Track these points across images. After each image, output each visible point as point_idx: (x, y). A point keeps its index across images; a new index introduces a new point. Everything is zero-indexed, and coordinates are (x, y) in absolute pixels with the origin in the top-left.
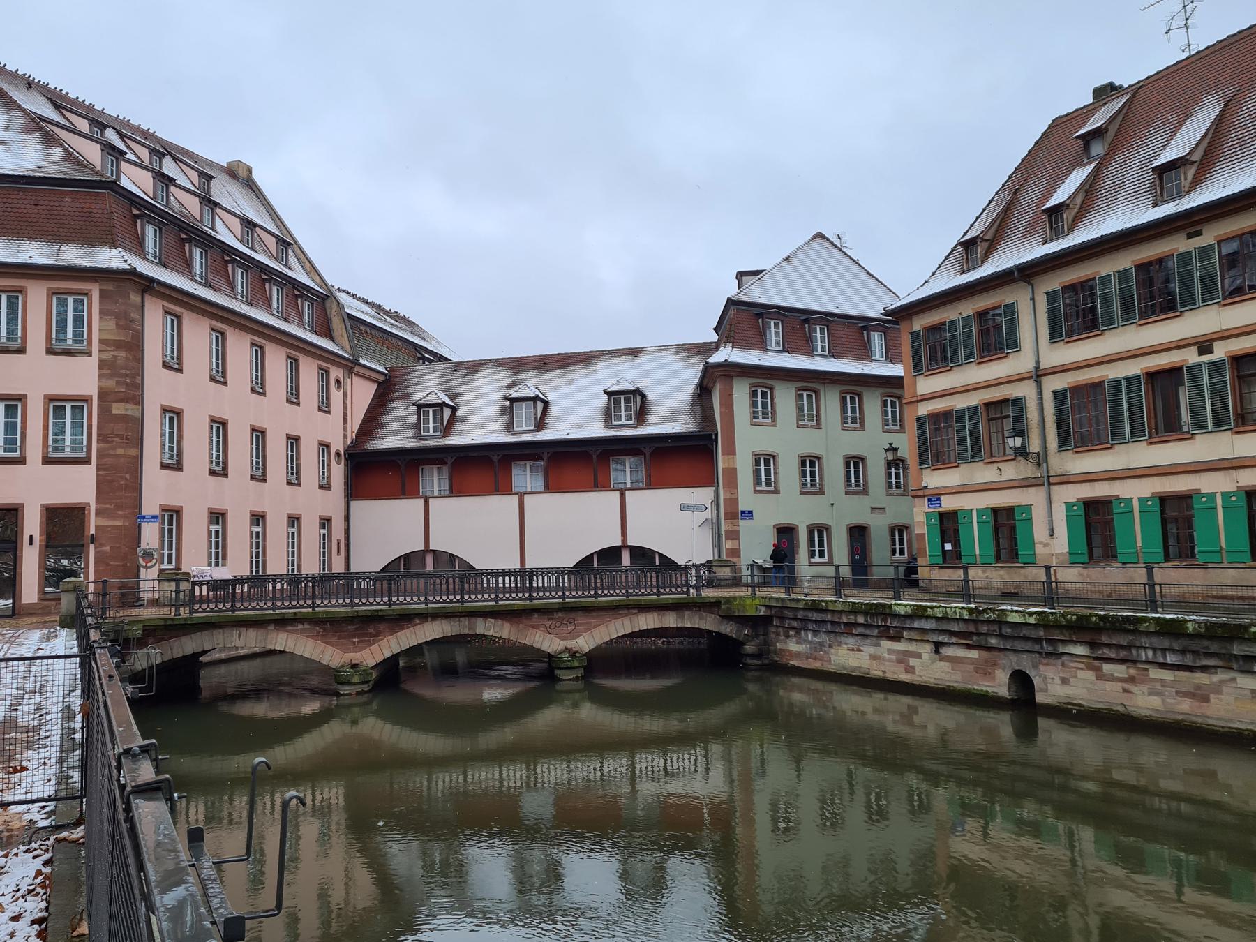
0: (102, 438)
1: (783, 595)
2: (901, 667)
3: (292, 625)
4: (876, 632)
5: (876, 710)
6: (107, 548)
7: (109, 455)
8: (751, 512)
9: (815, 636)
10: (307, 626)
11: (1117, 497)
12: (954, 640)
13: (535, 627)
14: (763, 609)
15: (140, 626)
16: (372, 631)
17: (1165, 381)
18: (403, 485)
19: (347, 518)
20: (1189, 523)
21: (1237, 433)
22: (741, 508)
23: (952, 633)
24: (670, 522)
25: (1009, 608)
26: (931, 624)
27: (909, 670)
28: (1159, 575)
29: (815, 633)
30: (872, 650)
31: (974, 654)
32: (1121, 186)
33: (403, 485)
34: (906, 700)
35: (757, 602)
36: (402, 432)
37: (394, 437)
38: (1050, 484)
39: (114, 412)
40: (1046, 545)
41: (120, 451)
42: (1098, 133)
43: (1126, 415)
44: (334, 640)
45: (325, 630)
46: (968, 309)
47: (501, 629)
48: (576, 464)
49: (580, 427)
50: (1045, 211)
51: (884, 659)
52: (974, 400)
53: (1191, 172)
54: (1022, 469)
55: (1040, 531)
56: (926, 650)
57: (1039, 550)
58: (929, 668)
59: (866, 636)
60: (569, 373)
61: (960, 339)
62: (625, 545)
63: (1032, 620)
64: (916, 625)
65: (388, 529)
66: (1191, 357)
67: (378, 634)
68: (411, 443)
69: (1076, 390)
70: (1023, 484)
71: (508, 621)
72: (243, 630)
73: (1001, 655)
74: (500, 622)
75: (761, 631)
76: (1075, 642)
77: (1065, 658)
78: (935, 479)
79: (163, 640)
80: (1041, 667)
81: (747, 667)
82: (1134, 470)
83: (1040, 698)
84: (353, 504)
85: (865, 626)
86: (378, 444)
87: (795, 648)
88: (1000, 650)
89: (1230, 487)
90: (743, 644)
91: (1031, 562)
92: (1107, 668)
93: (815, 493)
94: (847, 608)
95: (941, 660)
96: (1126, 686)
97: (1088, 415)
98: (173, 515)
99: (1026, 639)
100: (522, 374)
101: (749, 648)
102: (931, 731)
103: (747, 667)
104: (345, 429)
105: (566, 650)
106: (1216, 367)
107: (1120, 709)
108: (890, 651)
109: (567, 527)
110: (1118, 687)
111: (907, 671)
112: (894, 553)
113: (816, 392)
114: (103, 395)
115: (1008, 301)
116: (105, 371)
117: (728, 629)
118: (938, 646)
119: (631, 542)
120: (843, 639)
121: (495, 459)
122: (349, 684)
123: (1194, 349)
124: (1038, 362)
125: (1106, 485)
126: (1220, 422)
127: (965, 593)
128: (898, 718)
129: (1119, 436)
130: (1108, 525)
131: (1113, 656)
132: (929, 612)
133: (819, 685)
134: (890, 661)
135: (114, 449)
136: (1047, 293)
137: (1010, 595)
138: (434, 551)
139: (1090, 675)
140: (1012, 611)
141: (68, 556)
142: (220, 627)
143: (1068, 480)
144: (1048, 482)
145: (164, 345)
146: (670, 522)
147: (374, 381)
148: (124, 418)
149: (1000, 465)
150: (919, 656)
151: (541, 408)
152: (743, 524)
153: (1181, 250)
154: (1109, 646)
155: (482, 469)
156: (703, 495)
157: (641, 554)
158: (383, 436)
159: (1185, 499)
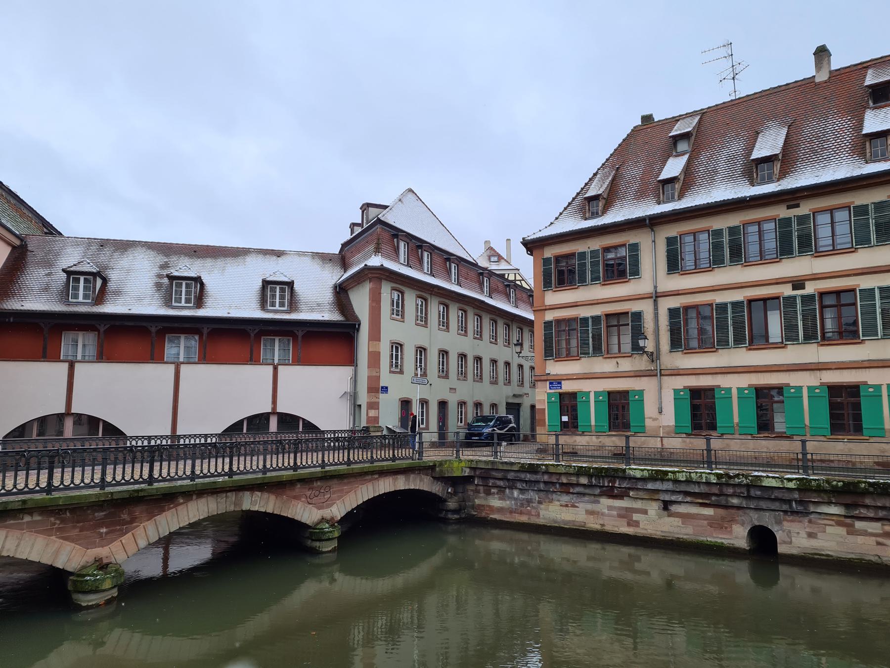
1: (492, 459)
2: (624, 522)
4: (597, 491)
5: (589, 558)
8: (387, 388)
9: (523, 494)
10: (37, 518)
11: (719, 386)
12: (689, 499)
13: (296, 498)
14: (468, 470)
17: (840, 298)
18: (45, 349)
20: (712, 408)
21: (822, 345)
22: (382, 384)
23: (687, 494)
24: (317, 393)
25: (764, 474)
26: (668, 486)
27: (637, 524)
28: (810, 446)
29: (522, 491)
30: (589, 507)
31: (709, 512)
32: (715, 172)
33: (45, 349)
34: (626, 551)
35: (463, 464)
36: (45, 296)
38: (661, 375)
40: (655, 419)
42: (685, 136)
43: (731, 329)
44: (75, 533)
45: (63, 521)
46: (595, 244)
47: (267, 503)
48: (230, 339)
50: (585, 198)
51: (603, 514)
52: (597, 311)
53: (678, 186)
54: (641, 363)
55: (650, 409)
56: (654, 508)
57: (648, 423)
58: (653, 521)
59: (584, 494)
60: (220, 262)
61: (588, 266)
62: (274, 412)
63: (791, 485)
64: (650, 486)
66: (787, 291)
67: (133, 520)
68: (57, 307)
69: (558, 322)
70: (638, 375)
71: (273, 493)
73: (740, 512)
74: (266, 495)
75: (460, 489)
76: (829, 503)
77: (812, 516)
78: (555, 368)
80: (785, 523)
81: (445, 521)
82: (730, 371)
83: (782, 549)
85: (590, 486)
86: (756, 154)
87: (496, 504)
88: (739, 508)
89: (816, 383)
90: (445, 501)
91: (642, 430)
92: (859, 525)
93: (443, 377)
94: (572, 470)
95: (669, 516)
96: (880, 540)
97: (692, 327)
99: (776, 499)
100: (174, 258)
101: (452, 504)
102: (656, 578)
103: (445, 521)
105: (323, 520)
106: (808, 299)
107: (874, 559)
108: (610, 508)
109: (221, 395)
110: (872, 541)
111: (629, 525)
113: (426, 300)
115: (632, 241)
117: (436, 488)
118: (666, 505)
119: (280, 409)
120: (554, 496)
121: (153, 330)
122: (96, 591)
123: (790, 286)
124: (656, 287)
125: (709, 377)
126: (810, 337)
127: (709, 460)
128: (616, 564)
129: (723, 343)
130: (625, 407)
131: (872, 515)
132: (670, 476)
133: (524, 536)
134: (609, 516)
136: (668, 239)
137: (769, 464)
139: (842, 531)
140: (768, 477)
143: (677, 373)
144: (657, 373)
146: (317, 393)
147: (9, 243)
149: (619, 360)
150: (645, 512)
151: (198, 289)
152: (382, 396)
153: (782, 216)
154: (867, 507)
156: (343, 373)
157: (288, 421)
158: (22, 298)
159: (854, 390)
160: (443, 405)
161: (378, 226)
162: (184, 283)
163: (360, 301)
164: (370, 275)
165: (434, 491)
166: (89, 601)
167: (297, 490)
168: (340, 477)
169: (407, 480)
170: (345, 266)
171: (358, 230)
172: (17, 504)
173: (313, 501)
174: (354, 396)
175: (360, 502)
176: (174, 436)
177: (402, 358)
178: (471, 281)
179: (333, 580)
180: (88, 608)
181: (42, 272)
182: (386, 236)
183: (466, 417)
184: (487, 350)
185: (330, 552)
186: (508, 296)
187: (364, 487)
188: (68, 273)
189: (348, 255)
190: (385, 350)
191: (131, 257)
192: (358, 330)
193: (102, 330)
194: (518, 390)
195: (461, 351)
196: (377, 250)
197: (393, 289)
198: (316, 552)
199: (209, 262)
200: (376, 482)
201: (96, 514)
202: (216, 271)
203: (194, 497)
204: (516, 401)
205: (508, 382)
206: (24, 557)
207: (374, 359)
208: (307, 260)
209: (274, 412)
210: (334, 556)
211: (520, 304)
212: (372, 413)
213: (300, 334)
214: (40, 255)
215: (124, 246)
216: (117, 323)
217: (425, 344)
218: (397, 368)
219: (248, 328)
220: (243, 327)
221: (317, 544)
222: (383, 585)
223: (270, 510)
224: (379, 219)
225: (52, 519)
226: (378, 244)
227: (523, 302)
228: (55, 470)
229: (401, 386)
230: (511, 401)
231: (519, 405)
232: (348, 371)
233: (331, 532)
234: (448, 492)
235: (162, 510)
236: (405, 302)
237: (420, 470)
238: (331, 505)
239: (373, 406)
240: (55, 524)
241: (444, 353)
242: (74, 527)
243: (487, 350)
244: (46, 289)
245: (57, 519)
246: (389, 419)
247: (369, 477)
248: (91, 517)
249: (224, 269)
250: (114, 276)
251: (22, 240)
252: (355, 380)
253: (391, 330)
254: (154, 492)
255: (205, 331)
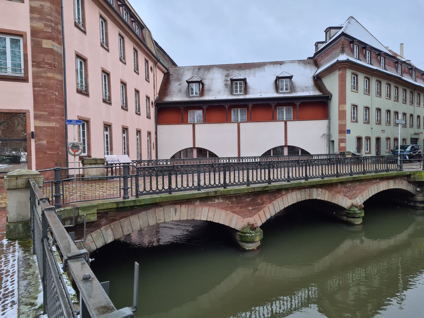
0: (36, 64)
3: (211, 200)
6: (44, 142)
7: (41, 77)
8: (350, 130)
10: (221, 201)
13: (339, 193)
15: (95, 211)
16: (259, 201)
19: (156, 133)
22: (347, 129)
37: (176, 96)
39: (44, 46)
41: (50, 75)
44: (237, 209)
45: (232, 203)
49: (264, 93)
60: (252, 71)
65: (176, 138)
67: (263, 203)
68: (186, 99)
71: (327, 189)
72: (178, 207)
74: (324, 191)
79: (114, 220)
84: (158, 126)
86: (168, 99)
98: (84, 123)
100: (231, 71)
103: (415, 208)
104: (154, 92)
105: (353, 206)
109: (261, 137)
112: (105, 154)
114: (34, 32)
116: (35, 15)
117: (410, 188)
119: (289, 144)
121: (227, 107)
135: (46, 73)
138: (197, 148)
141: (15, 150)
142: (161, 206)
145: (75, 14)
146: (308, 135)
148: (51, 51)
152: (347, 135)
155: (216, 111)
156: (322, 124)
157: (293, 150)
160: (378, 140)
161: (343, 37)
162: (238, 82)
163: (332, 84)
164: (339, 67)
165: (408, 190)
166: (249, 247)
167: (339, 188)
168: (360, 181)
169: (395, 183)
170: (317, 64)
171: (321, 46)
172: (213, 193)
173: (347, 195)
174: (329, 136)
175: (371, 196)
176: (239, 158)
177: (357, 114)
178: (392, 67)
179: (362, 241)
180: (249, 251)
181: (177, 84)
182: (347, 43)
183: (390, 147)
184: (402, 107)
185: (360, 224)
186: (411, 75)
187: (372, 187)
188: (189, 82)
189: (319, 59)
190: (348, 108)
191: (212, 73)
192: (330, 99)
193: (205, 108)
194: (417, 131)
195: (387, 109)
196: (343, 51)
197: (353, 74)
198: (351, 224)
199: (247, 71)
200: (378, 184)
201: (247, 199)
202: (251, 75)
203: (290, 191)
204: (416, 137)
205: (412, 126)
206: (217, 221)
207: (342, 115)
208: (296, 65)
209: (286, 146)
210: (361, 227)
211: (418, 80)
212: (342, 145)
213: (298, 104)
214: (175, 76)
215: (208, 68)
216: (211, 104)
217: (369, 106)
218: (355, 120)
219: (271, 103)
220: (268, 102)
221: (352, 220)
222: (384, 244)
223: (326, 199)
224: (83, 165)
225: (228, 202)
226: (343, 48)
227: (419, 78)
228: (201, 174)
229: (358, 129)
230: (413, 137)
231: (417, 139)
232: (325, 123)
233: (360, 213)
234: (416, 191)
235: (276, 198)
236: (359, 81)
237: (401, 177)
238: (356, 197)
239: (342, 141)
240: (229, 204)
241: (379, 110)
242: (237, 206)
243: (402, 107)
244: (180, 91)
245: (229, 201)
246: (351, 147)
247: (375, 181)
248: (244, 201)
249: (264, 70)
250: (206, 82)
251: (167, 70)
252: (329, 128)
253: (351, 97)
254: (273, 188)
255: (250, 106)
